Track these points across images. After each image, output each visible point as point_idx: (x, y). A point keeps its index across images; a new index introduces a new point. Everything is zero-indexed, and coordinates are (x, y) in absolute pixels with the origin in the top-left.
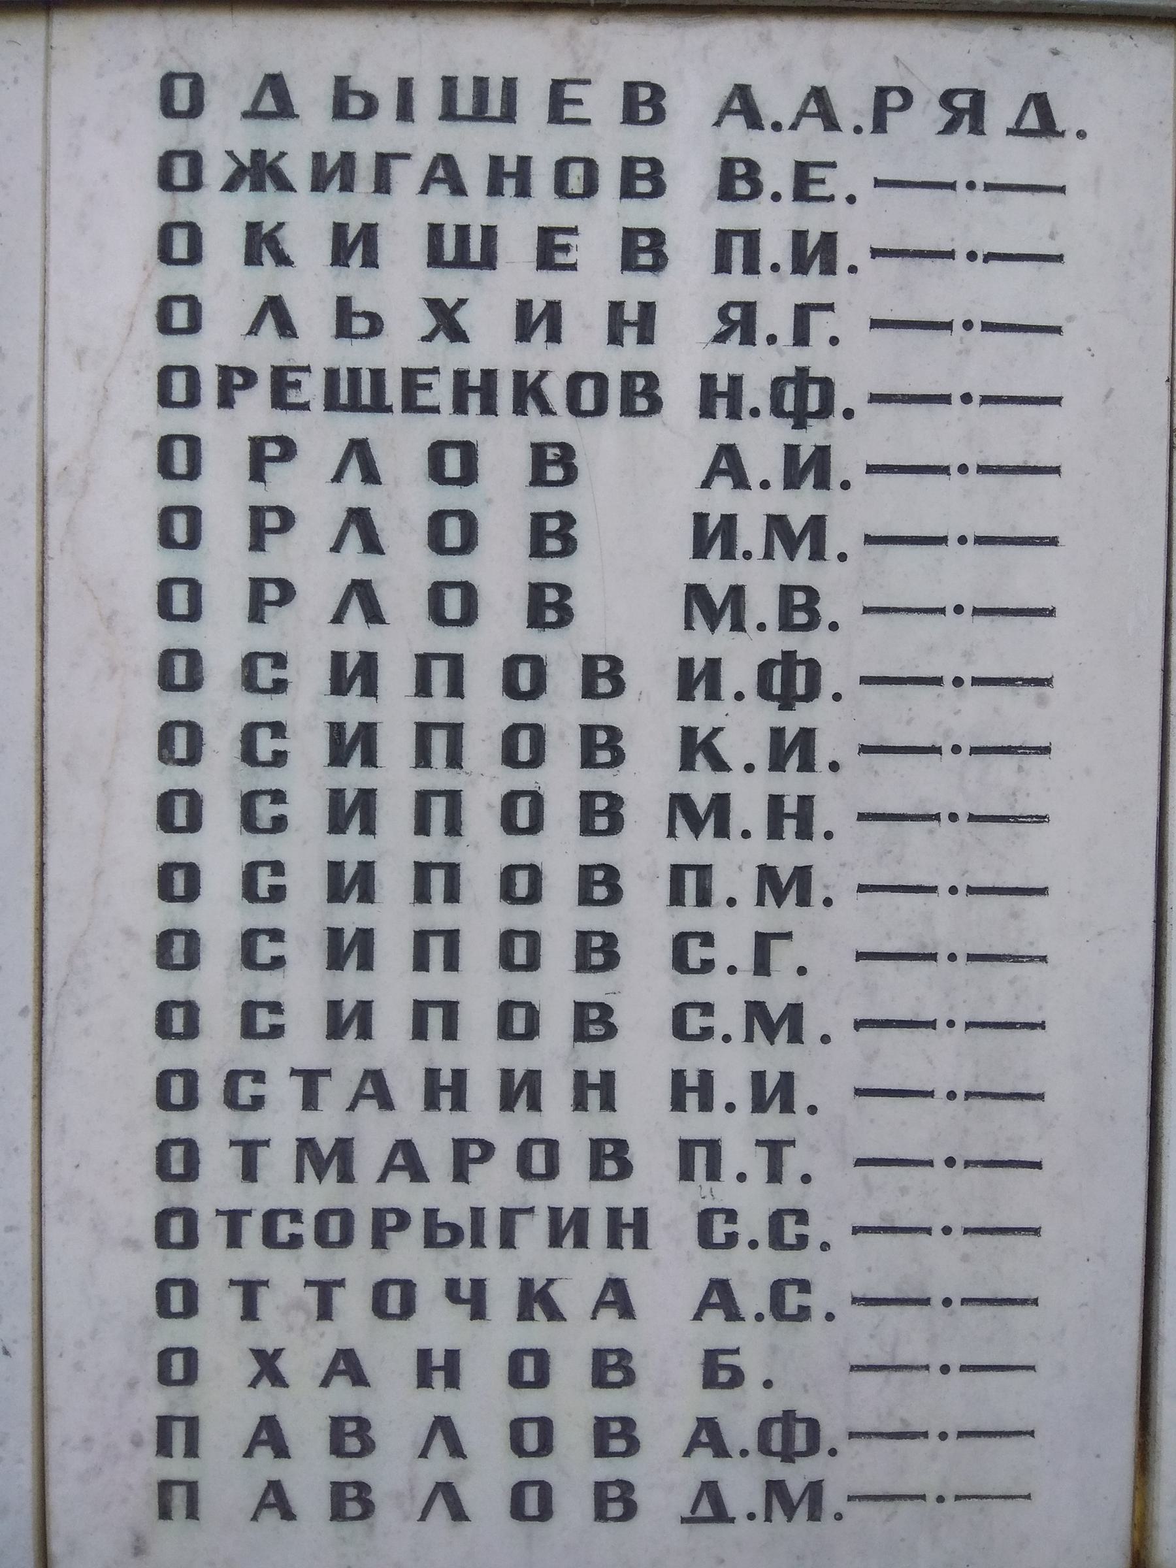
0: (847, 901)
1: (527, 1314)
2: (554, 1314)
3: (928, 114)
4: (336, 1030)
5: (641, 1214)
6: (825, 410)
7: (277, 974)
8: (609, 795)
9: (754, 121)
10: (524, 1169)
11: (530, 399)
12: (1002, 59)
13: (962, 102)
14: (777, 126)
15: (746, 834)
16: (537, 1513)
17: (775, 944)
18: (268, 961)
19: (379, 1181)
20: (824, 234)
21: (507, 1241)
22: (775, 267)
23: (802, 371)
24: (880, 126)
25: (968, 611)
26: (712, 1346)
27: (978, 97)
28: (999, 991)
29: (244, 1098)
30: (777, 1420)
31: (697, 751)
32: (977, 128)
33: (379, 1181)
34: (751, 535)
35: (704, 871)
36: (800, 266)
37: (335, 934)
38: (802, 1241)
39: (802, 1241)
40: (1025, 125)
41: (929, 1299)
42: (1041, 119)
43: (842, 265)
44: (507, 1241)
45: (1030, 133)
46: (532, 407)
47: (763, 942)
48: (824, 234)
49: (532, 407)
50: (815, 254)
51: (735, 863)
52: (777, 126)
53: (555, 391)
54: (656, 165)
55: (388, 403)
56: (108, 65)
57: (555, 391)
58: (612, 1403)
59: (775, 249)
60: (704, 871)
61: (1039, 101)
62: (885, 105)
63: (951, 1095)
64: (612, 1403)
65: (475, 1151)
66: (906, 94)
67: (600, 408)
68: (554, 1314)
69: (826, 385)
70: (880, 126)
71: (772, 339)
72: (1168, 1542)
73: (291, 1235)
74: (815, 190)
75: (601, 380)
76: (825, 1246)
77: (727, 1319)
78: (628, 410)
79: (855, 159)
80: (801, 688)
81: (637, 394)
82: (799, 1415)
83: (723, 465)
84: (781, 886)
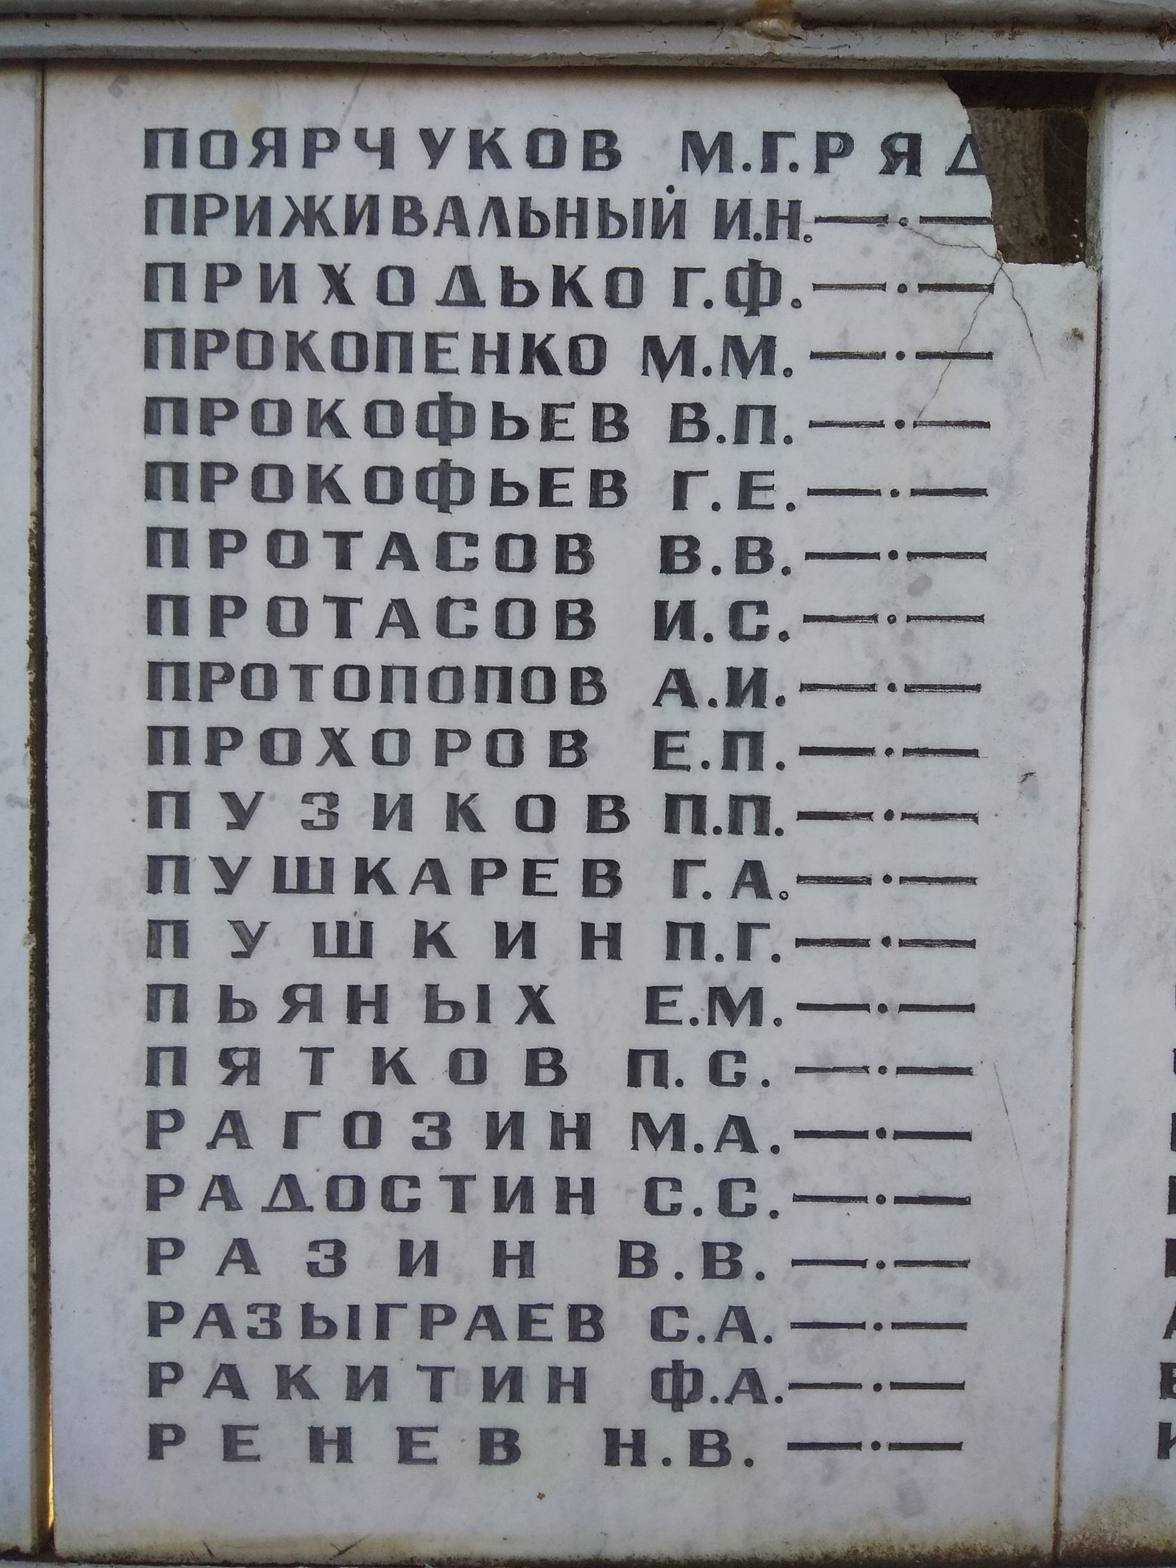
3: (868, 155)
4: (354, 1392)
10: (274, 626)
14: (714, 1400)
15: (699, 1148)
19: (342, 401)
20: (354, 233)
22: (794, 167)
24: (822, 167)
27: (915, 140)
32: (914, 169)
33: (342, 401)
34: (708, 352)
35: (756, 738)
38: (740, 1078)
39: (740, 1078)
40: (452, 297)
45: (457, 303)
47: (745, 930)
48: (354, 233)
50: (754, 554)
52: (714, 1400)
53: (322, 349)
55: (482, 299)
56: (100, 128)
57: (322, 349)
59: (721, 421)
60: (756, 738)
62: (831, 149)
70: (822, 167)
74: (672, 759)
80: (764, 296)
81: (406, 215)
83: (748, 878)
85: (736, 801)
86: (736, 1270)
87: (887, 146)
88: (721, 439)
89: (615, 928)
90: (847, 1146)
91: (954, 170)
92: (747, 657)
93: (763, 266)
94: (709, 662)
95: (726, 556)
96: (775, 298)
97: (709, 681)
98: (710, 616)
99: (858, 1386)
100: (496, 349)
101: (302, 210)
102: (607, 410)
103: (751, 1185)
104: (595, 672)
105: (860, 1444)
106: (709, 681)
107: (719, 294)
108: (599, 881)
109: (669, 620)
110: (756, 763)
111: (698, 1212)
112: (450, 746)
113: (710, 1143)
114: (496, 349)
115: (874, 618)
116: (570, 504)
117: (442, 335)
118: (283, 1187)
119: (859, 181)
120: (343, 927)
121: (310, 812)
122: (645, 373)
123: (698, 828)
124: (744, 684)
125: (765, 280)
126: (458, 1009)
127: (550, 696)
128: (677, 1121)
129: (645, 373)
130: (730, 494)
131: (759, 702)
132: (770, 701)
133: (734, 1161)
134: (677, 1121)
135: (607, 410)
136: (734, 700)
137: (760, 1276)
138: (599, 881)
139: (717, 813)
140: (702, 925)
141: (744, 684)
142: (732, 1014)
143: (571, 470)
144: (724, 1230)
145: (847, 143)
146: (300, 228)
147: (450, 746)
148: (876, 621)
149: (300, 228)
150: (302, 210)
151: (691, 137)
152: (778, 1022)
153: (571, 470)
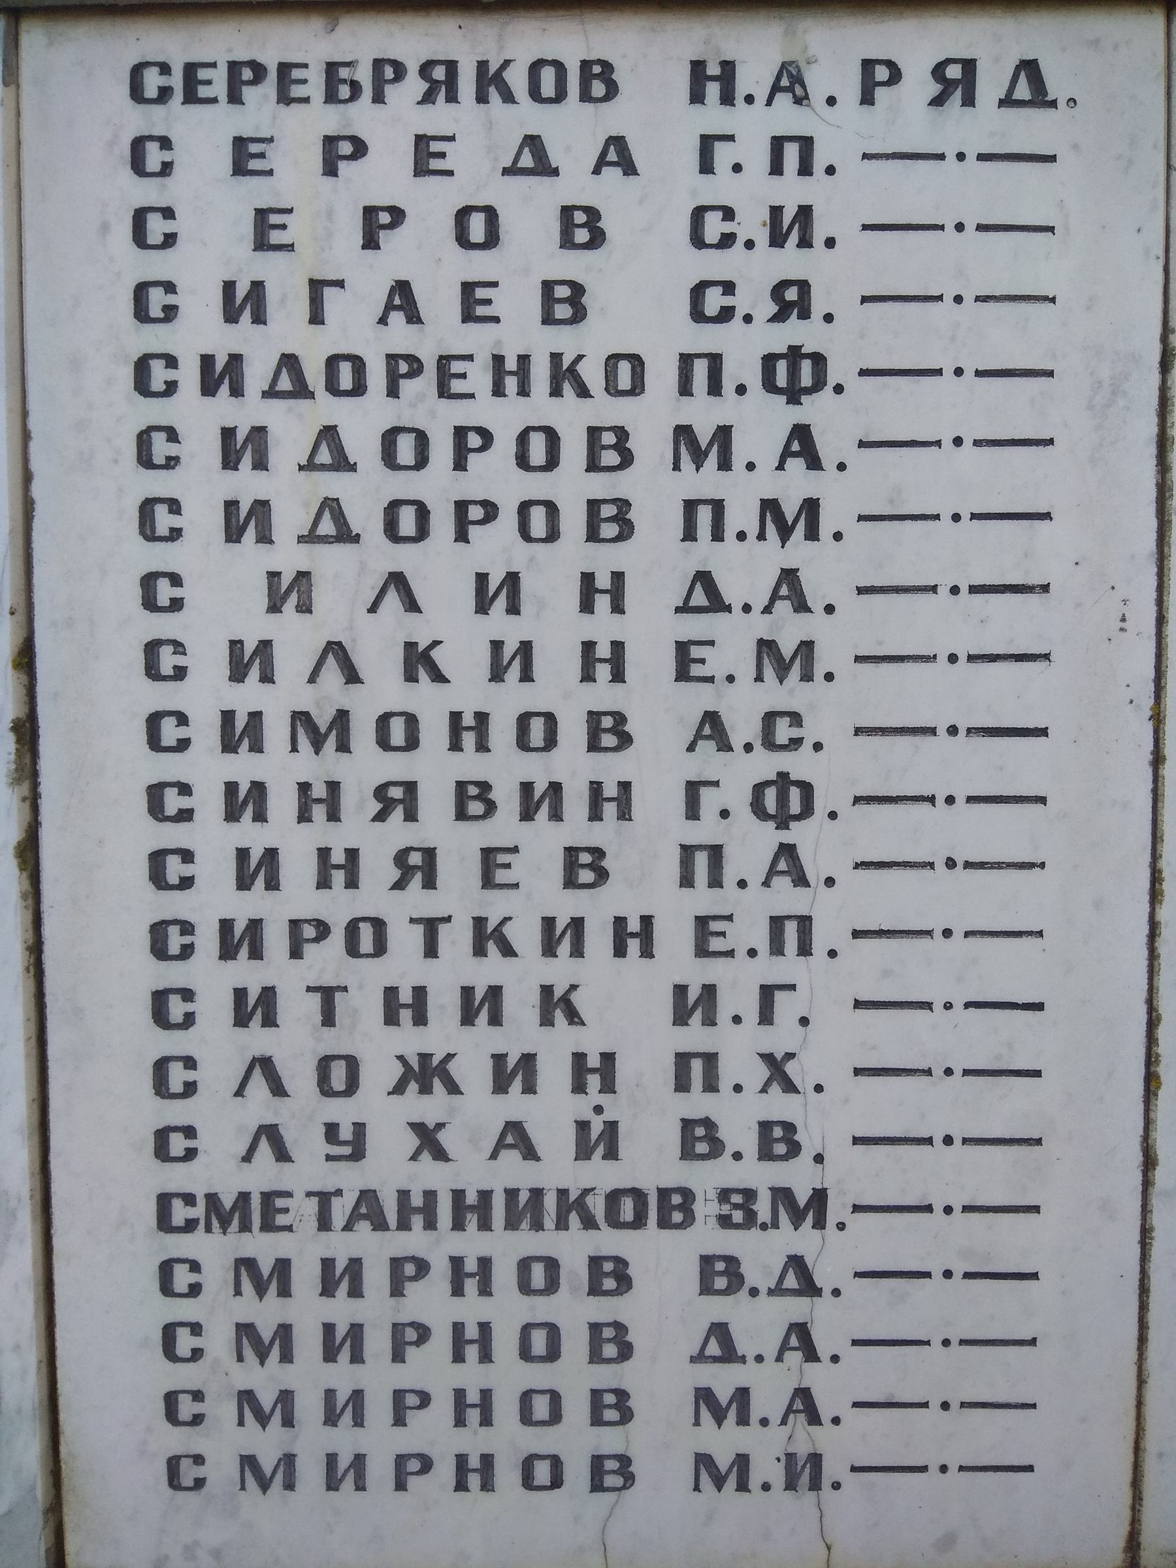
1: (562, 1226)
2: (508, 951)
3: (918, 84)
5: (608, 1058)
6: (807, 810)
7: (183, 826)
8: (600, 62)
12: (994, 43)
13: (954, 72)
14: (764, 1422)
15: (766, 1487)
16: (541, 744)
17: (779, 996)
18: (174, 743)
23: (783, 776)
24: (867, 99)
26: (694, 778)
27: (969, 66)
28: (1005, 1108)
29: (155, 237)
32: (969, 100)
37: (260, 464)
42: (1031, 86)
43: (832, 1219)
46: (494, 94)
47: (767, 993)
49: (494, 94)
53: (517, 79)
56: (79, 74)
57: (517, 79)
61: (1030, 68)
62: (877, 76)
65: (410, 1269)
68: (508, 951)
69: (818, 359)
73: (191, 1286)
76: (818, 747)
79: (840, 131)
82: (793, 777)
85: (777, 923)
87: (938, 71)
88: (737, 1156)
89: (618, 577)
91: (1007, 102)
92: (779, 1106)
95: (749, 1143)
99: (937, 517)
100: (597, 596)
107: (753, 378)
108: (604, 526)
109: (246, 943)
112: (576, 222)
113: (755, 879)
114: (411, 1002)
117: (716, 918)
118: (698, 586)
119: (908, 110)
122: (294, 749)
123: (718, 535)
128: (742, 1395)
129: (294, 749)
134: (742, 1395)
138: (604, 526)
140: (809, 918)
142: (797, 1218)
145: (895, 76)
146: (413, 1087)
147: (576, 222)
148: (756, 680)
149: (413, 1087)
152: (838, 536)
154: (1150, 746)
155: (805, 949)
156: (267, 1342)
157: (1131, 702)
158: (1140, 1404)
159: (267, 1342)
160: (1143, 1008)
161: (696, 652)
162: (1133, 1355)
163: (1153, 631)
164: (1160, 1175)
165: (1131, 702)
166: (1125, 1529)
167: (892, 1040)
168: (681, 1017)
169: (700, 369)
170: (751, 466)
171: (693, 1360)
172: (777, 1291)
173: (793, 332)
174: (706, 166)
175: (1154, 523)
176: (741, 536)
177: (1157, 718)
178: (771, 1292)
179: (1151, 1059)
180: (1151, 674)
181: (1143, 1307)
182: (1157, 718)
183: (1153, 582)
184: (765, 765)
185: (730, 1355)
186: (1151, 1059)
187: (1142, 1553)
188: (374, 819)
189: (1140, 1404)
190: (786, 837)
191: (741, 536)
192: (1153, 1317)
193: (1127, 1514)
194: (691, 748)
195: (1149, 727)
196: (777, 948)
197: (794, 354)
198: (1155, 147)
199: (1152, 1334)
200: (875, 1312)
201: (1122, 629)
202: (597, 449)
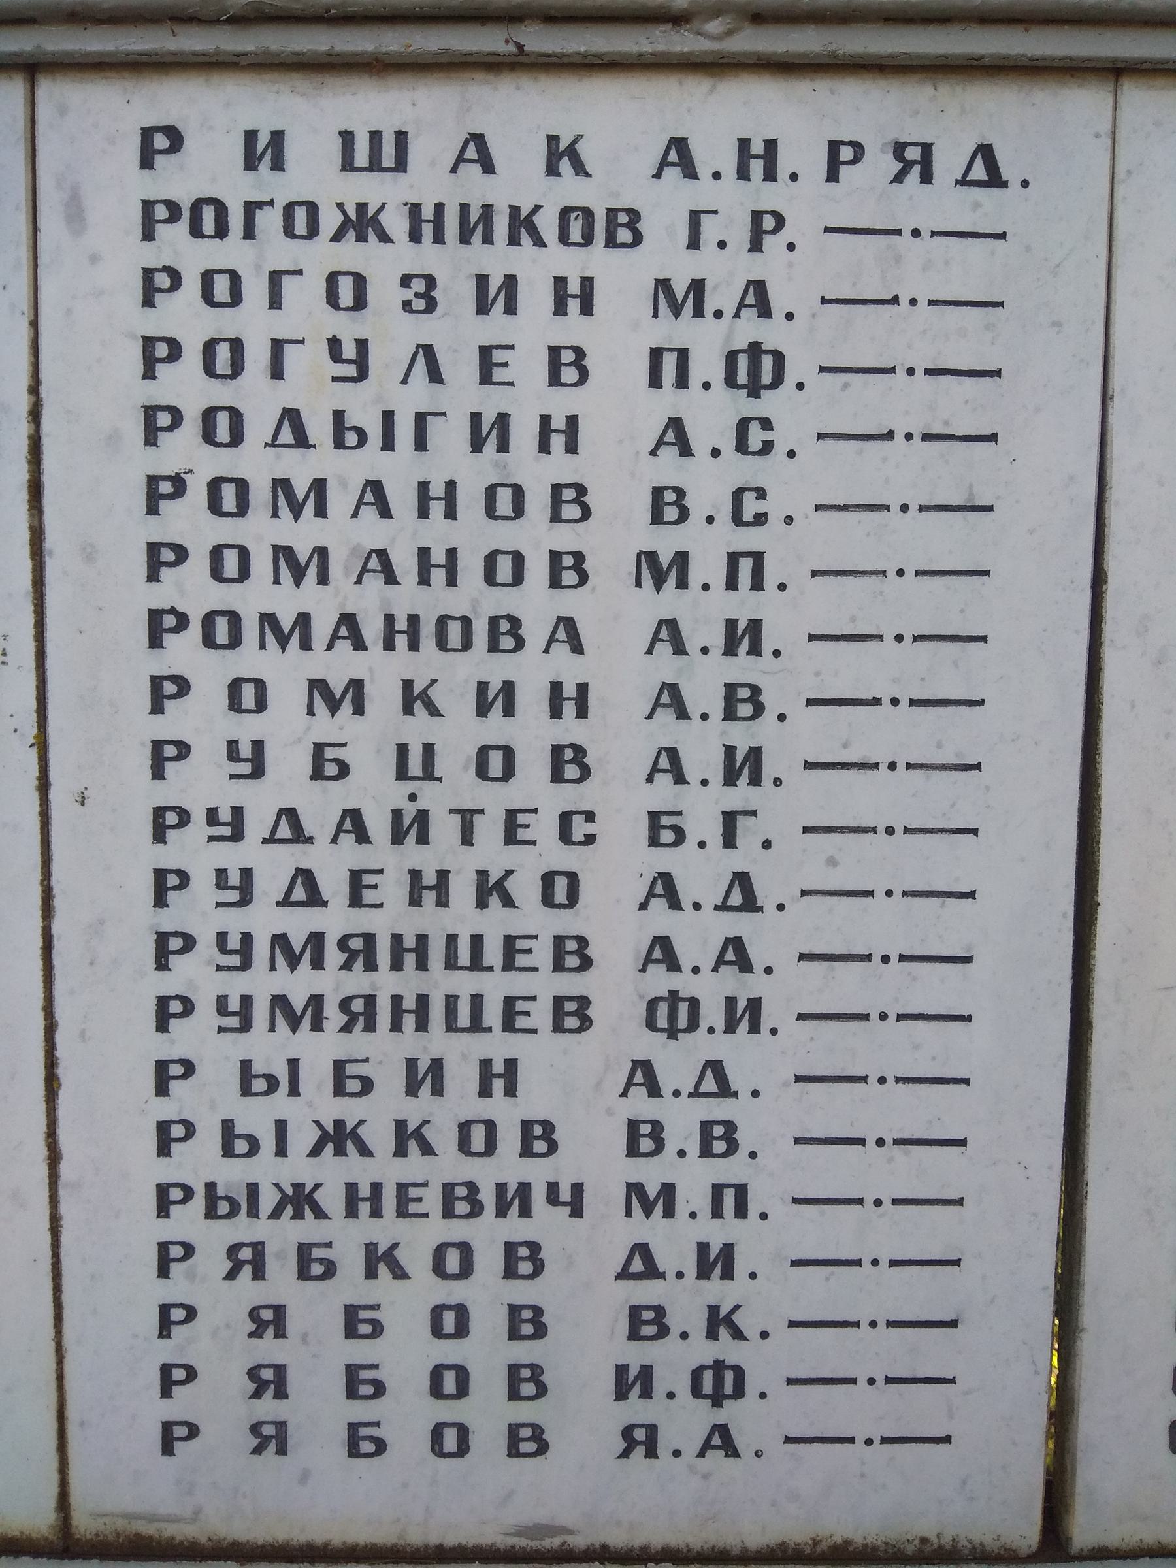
0: (790, 1028)
9: (654, 1090)
11: (523, 230)
12: (956, 120)
21: (249, 233)
25: (892, 1017)
27: (927, 149)
30: (729, 1397)
31: (520, 227)
36: (704, 1272)
40: (972, 176)
41: (894, 368)
42: (988, 171)
44: (249, 233)
46: (525, 239)
47: (730, 819)
51: (703, 748)
53: (548, 224)
54: (538, 1311)
56: (95, 121)
57: (548, 224)
58: (523, 1292)
61: (986, 152)
62: (838, 159)
63: (899, 638)
64: (523, 1292)
66: (858, 148)
67: (588, 239)
71: (682, 1153)
72: (1084, 1530)
75: (588, 213)
77: (713, 1406)
78: (611, 242)
84: (744, 766)
86: (732, 1147)
87: (899, 149)
90: (833, 969)
91: (963, 182)
93: (764, 347)
94: (704, 611)
96: (777, 381)
97: (703, 693)
98: (707, 566)
101: (354, 217)
102: (501, 621)
103: (761, 493)
104: (579, 750)
105: (894, 368)
106: (703, 693)
110: (757, 584)
111: (696, 970)
113: (706, 965)
115: (890, 435)
116: (380, 905)
119: (867, 188)
120: (375, 137)
121: (408, 294)
124: (746, 640)
125: (767, 362)
126: (272, 1083)
127: (467, 645)
130: (740, 235)
131: (755, 780)
132: (767, 781)
133: (749, 329)
135: (501, 621)
136: (730, 779)
137: (755, 1094)
139: (712, 1013)
141: (746, 640)
143: (512, 347)
144: (716, 1234)
150: (354, 217)
151: (663, 285)
153: (512, 347)
154: (35, 772)
155: (741, 1211)
156: (338, 696)
157: (16, 731)
158: (60, 1378)
159: (338, 696)
160: (40, 1015)
161: (522, 819)
162: (51, 1332)
163: (33, 665)
164: (64, 1168)
165: (16, 731)
166: (54, 1490)
167: (847, 671)
168: (621, 1393)
169: (729, 1198)
170: (706, 587)
171: (619, 1277)
172: (695, 1094)
173: (726, 1349)
174: (694, 243)
175: (28, 564)
176: (718, 314)
177: (42, 745)
178: (690, 1095)
179: (51, 1063)
180: (33, 704)
181: (57, 1289)
182: (42, 745)
183: (29, 619)
184: (749, 329)
185: (652, 1272)
186: (51, 1063)
187: (72, 1513)
188: (342, 968)
189: (60, 1378)
190: (721, 1416)
191: (718, 314)
192: (66, 1298)
193: (55, 1477)
194: (650, 780)
195: (33, 755)
196: (717, 1213)
197: (719, 1367)
198: (17, 208)
199: (67, 1313)
200: (834, 606)
201: (3, 663)
202: (522, 59)
